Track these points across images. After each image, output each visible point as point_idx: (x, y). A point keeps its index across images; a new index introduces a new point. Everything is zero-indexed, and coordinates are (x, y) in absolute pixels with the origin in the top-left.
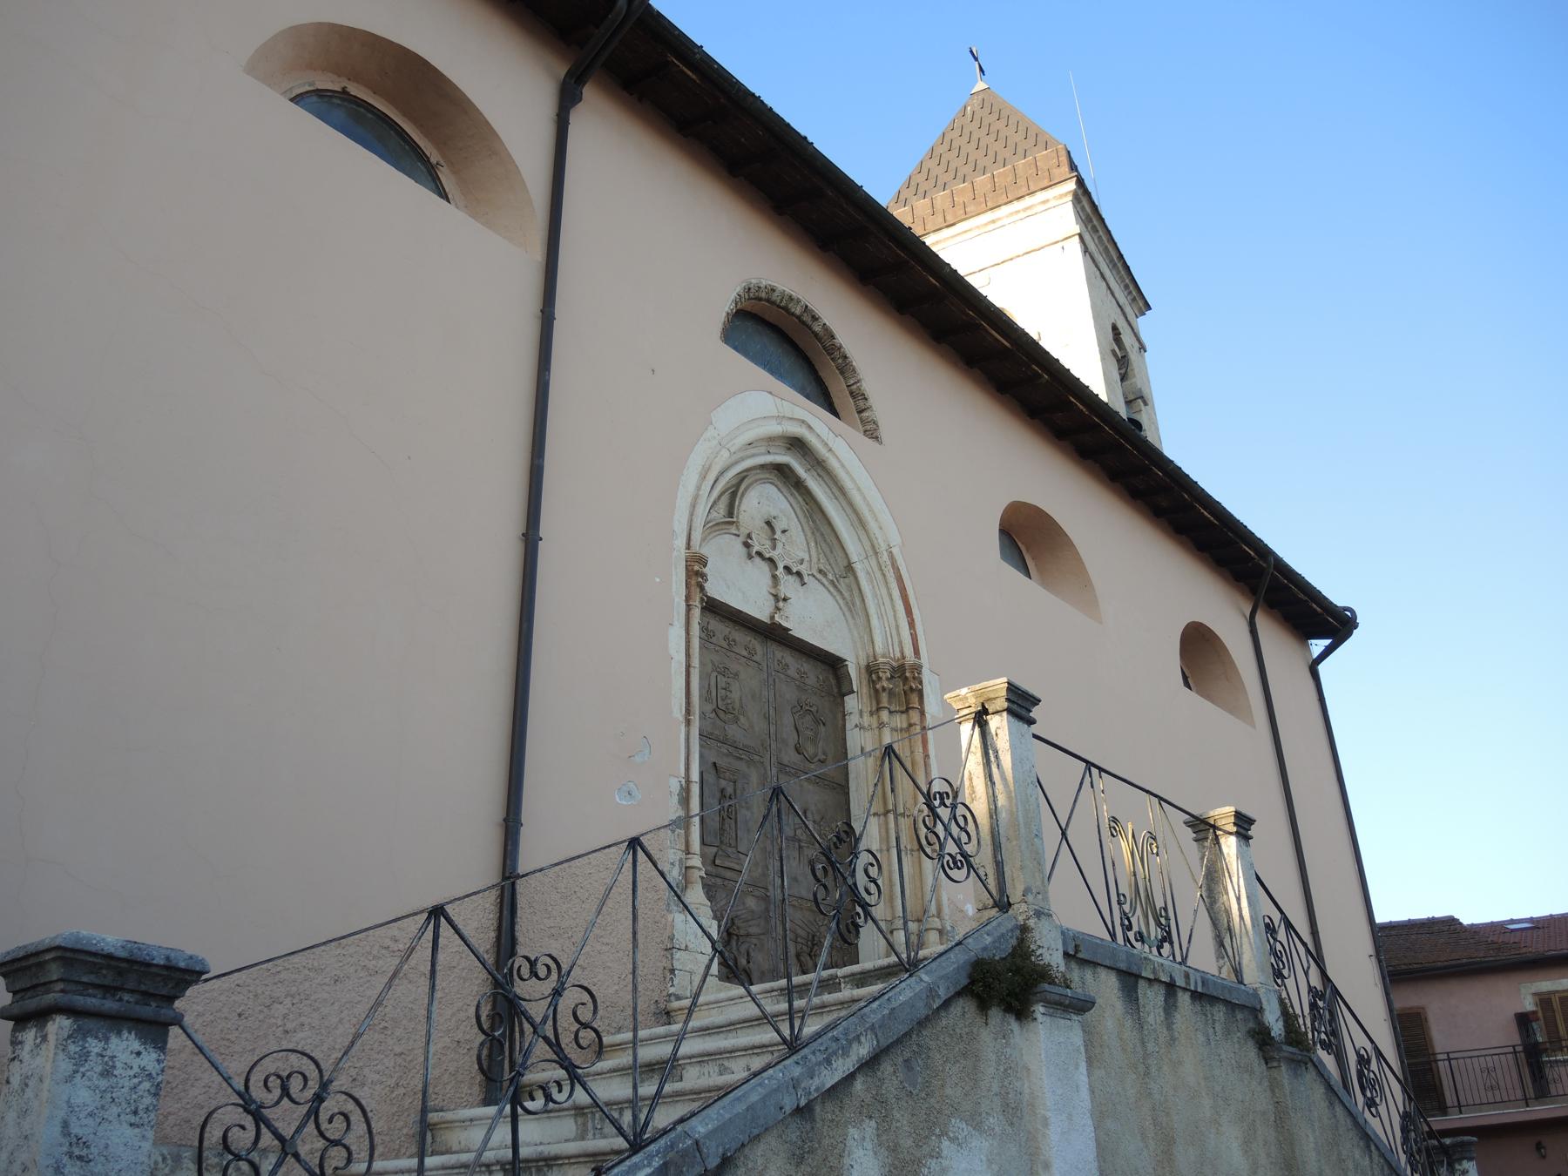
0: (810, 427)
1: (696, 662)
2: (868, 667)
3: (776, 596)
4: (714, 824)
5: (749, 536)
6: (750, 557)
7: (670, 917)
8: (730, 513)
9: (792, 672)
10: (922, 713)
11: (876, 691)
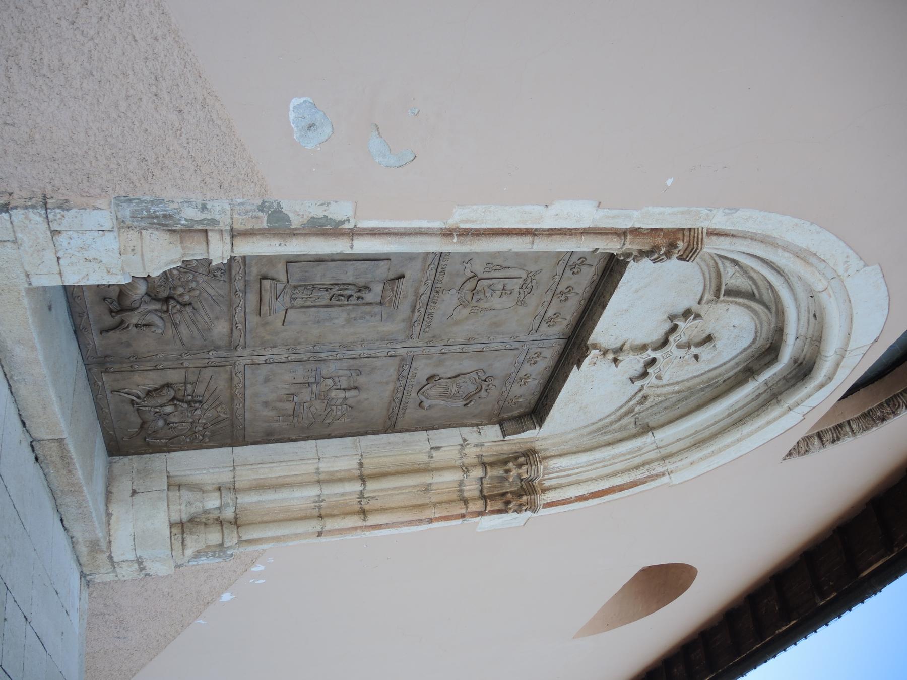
0: (822, 386)
1: (541, 245)
2: (533, 452)
3: (621, 349)
4: (321, 276)
5: (698, 316)
6: (672, 318)
7: (101, 203)
8: (729, 293)
9: (527, 368)
10: (480, 514)
11: (505, 462)
